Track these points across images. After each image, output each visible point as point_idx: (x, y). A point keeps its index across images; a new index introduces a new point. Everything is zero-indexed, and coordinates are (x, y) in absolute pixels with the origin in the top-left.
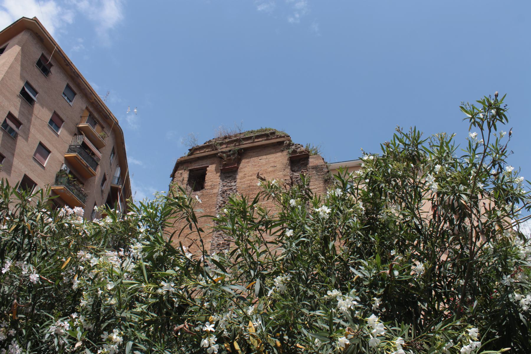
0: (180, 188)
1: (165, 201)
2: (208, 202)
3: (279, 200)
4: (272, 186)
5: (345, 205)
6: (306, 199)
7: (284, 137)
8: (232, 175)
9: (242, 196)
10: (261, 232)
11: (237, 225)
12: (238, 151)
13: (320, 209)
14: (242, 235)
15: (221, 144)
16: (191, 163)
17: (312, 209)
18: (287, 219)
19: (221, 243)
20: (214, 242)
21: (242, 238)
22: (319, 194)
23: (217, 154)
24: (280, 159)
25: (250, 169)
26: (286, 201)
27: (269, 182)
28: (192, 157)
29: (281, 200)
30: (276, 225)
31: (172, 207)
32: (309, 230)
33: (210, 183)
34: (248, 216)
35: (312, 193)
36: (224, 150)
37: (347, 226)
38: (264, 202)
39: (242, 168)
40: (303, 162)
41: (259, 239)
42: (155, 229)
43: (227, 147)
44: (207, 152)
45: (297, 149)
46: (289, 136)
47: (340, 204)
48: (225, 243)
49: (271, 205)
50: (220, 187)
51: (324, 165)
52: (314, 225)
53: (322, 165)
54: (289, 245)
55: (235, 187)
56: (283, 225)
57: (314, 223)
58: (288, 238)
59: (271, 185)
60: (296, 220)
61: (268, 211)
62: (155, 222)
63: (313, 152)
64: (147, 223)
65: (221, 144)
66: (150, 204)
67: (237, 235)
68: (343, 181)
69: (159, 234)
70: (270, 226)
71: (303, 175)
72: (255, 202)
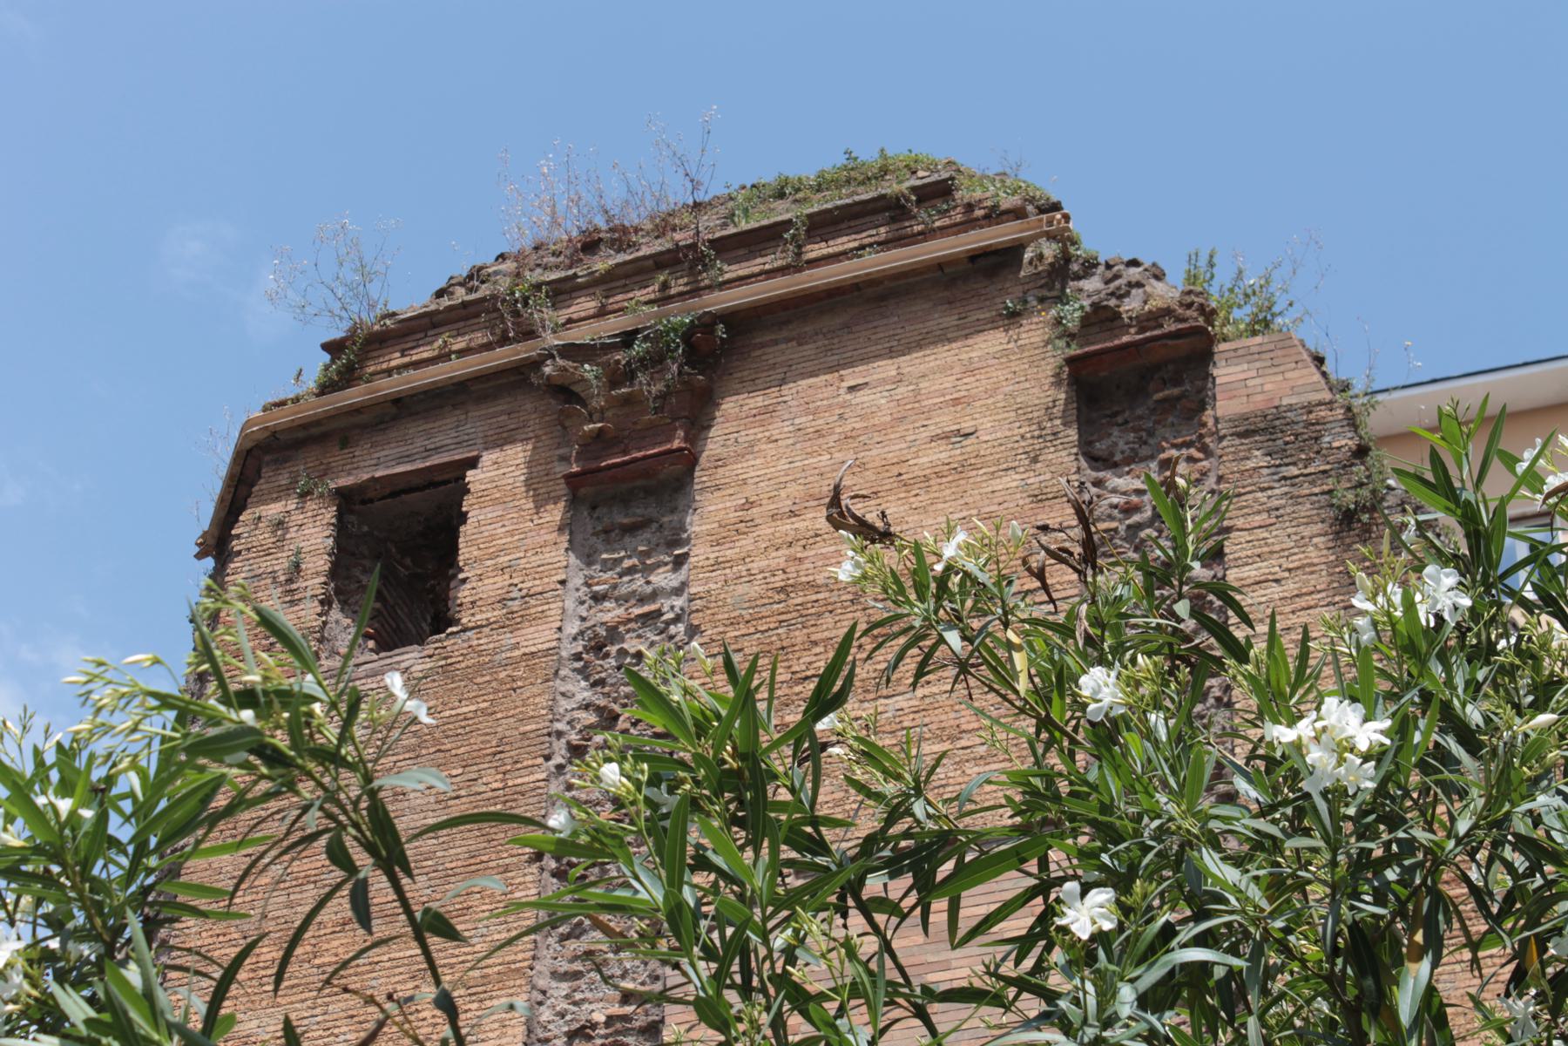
0: (267, 623)
1: (162, 723)
2: (485, 724)
3: (1004, 676)
4: (942, 582)
5: (1496, 686)
6: (1204, 664)
7: (1018, 213)
8: (652, 511)
9: (729, 666)
10: (880, 918)
11: (703, 879)
12: (688, 334)
13: (1304, 729)
14: (742, 949)
15: (561, 292)
16: (345, 443)
17: (1254, 734)
18: (1073, 818)
19: (599, 1017)
20: (546, 1015)
21: (746, 972)
22: (1303, 618)
23: (536, 364)
24: (1001, 375)
25: (783, 465)
26: (1061, 680)
27: (917, 549)
28: (354, 395)
29: (1015, 675)
30: (989, 866)
31: (215, 769)
32: (1236, 890)
33: (492, 586)
34: (782, 807)
35: (1246, 619)
36: (582, 335)
37: (1522, 843)
38: (901, 702)
39: (720, 462)
40: (1176, 391)
41: (870, 973)
42: (97, 938)
43: (602, 313)
44: (462, 353)
45: (1120, 296)
46: (1056, 207)
47: (1459, 681)
48: (625, 1018)
49: (949, 719)
50: (570, 604)
51: (1330, 404)
52: (1276, 845)
53: (1309, 408)
54: (1091, 1001)
55: (679, 602)
56: (1044, 863)
57: (1273, 830)
58: (1084, 955)
59: (939, 568)
60: (1138, 819)
61: (929, 761)
62: (98, 886)
63: (1242, 314)
64: (39, 902)
65: (561, 292)
66: (50, 757)
67: (709, 953)
68: (1469, 516)
69: (133, 974)
70: (948, 867)
71: (1170, 485)
72: (824, 702)
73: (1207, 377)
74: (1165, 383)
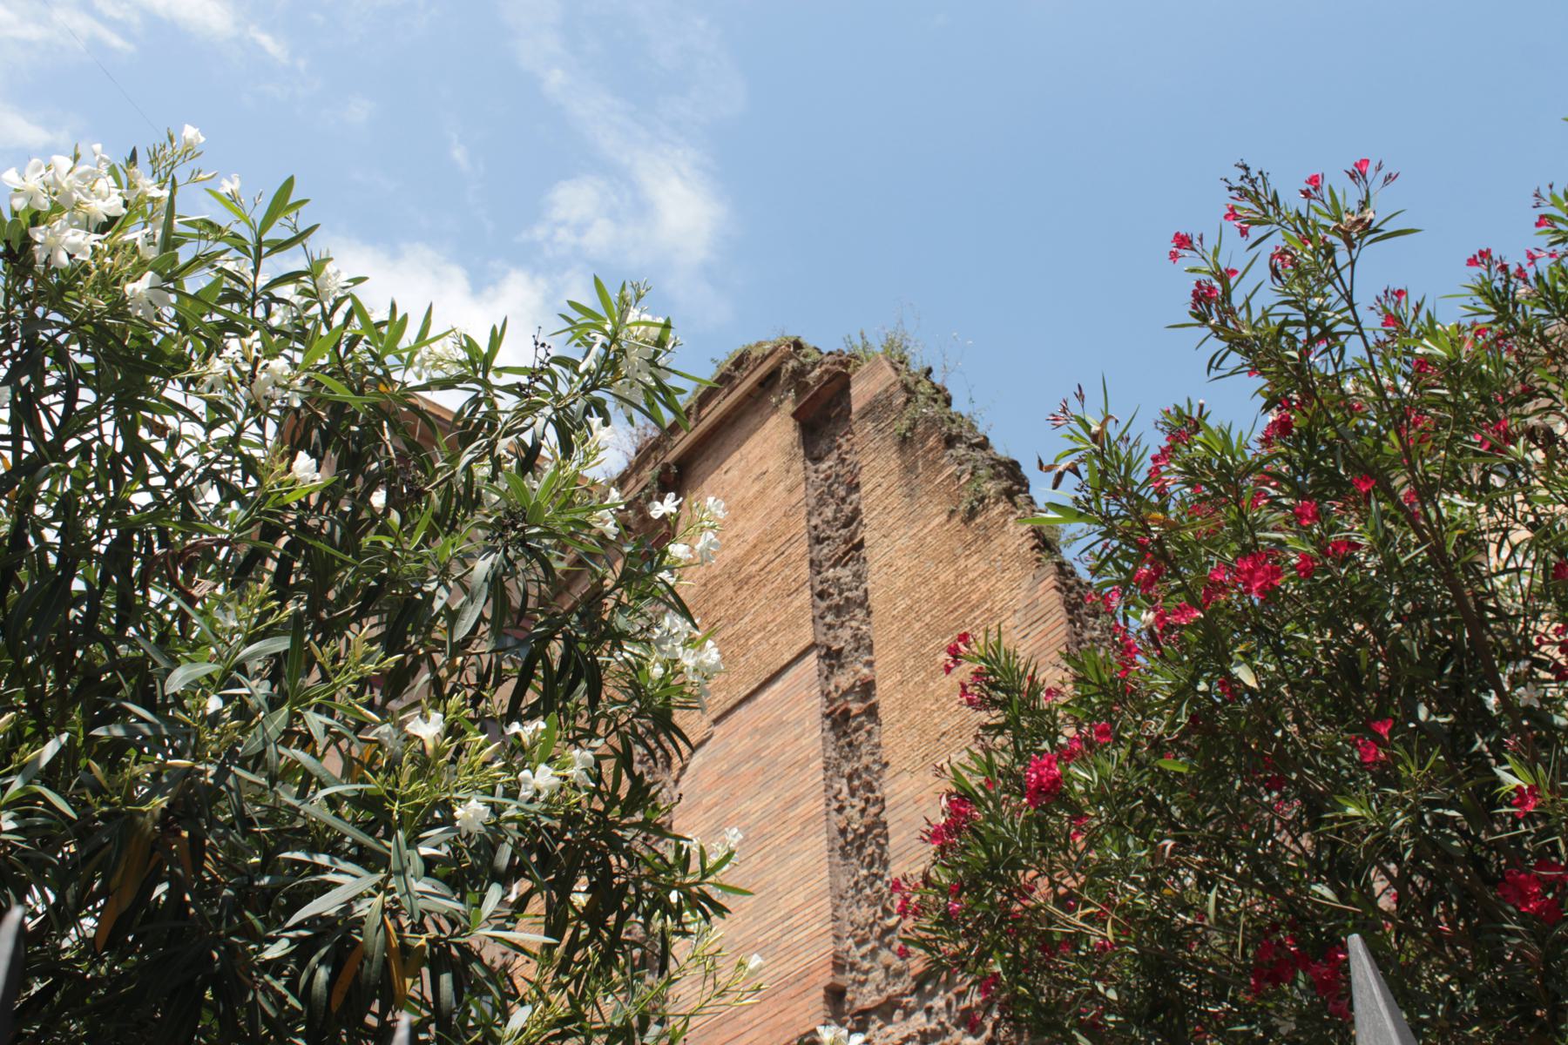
73: (849, 395)
74: (836, 406)
